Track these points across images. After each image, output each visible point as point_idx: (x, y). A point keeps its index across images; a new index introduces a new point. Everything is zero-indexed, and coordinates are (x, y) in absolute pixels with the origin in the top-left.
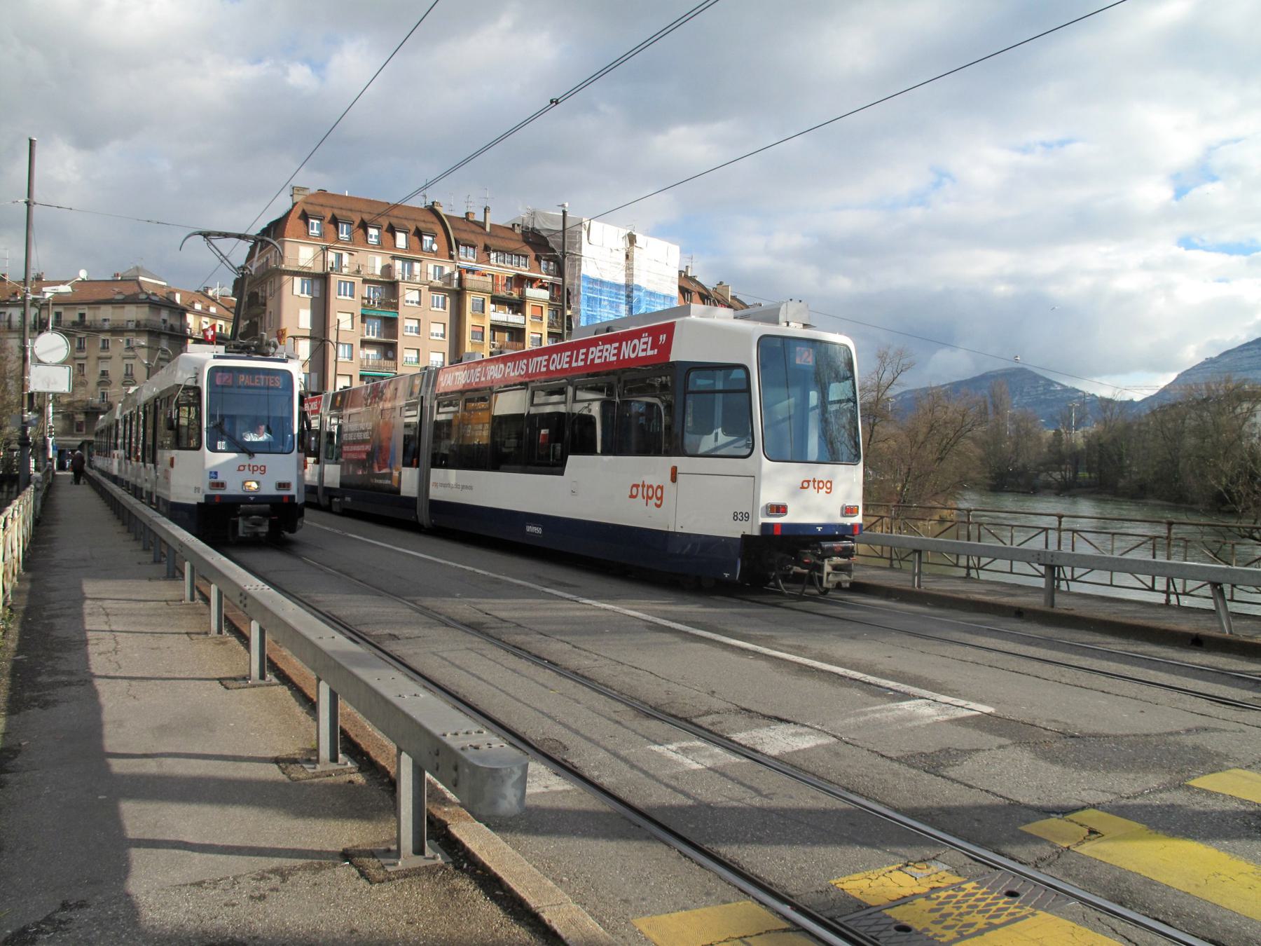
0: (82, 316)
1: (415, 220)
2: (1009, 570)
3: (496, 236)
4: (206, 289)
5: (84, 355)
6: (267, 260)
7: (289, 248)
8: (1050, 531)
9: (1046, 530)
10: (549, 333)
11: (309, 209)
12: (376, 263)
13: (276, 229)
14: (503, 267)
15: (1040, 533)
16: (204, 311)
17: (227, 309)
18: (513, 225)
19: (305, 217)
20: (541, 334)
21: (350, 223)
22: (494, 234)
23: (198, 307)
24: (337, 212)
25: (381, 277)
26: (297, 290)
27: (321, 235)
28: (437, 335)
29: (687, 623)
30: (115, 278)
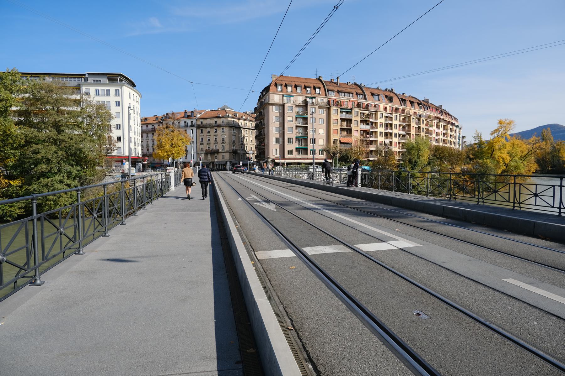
0: (202, 122)
1: (313, 83)
2: (494, 199)
3: (341, 87)
4: (247, 112)
5: (210, 134)
6: (264, 100)
7: (271, 96)
8: (555, 187)
9: (554, 186)
10: (361, 120)
11: (278, 82)
12: (300, 100)
13: (267, 89)
14: (344, 98)
15: (507, 184)
16: (246, 119)
17: (253, 118)
18: (348, 82)
19: (276, 85)
20: (337, 119)
21: (301, 87)
22: (341, 86)
23: (244, 117)
24: (287, 82)
25: (302, 104)
26: (274, 110)
27: (301, 92)
28: (290, 121)
29: (446, 223)
30: (218, 109)
